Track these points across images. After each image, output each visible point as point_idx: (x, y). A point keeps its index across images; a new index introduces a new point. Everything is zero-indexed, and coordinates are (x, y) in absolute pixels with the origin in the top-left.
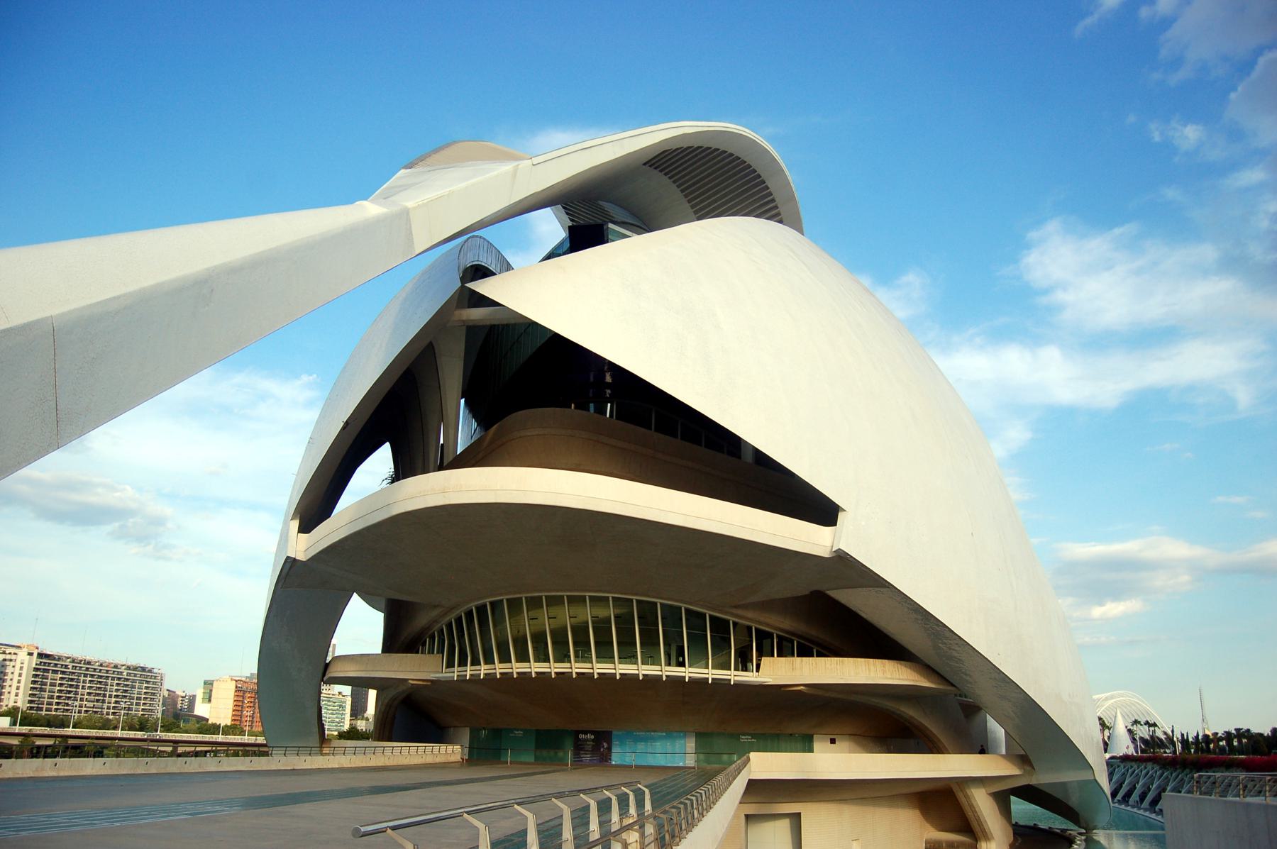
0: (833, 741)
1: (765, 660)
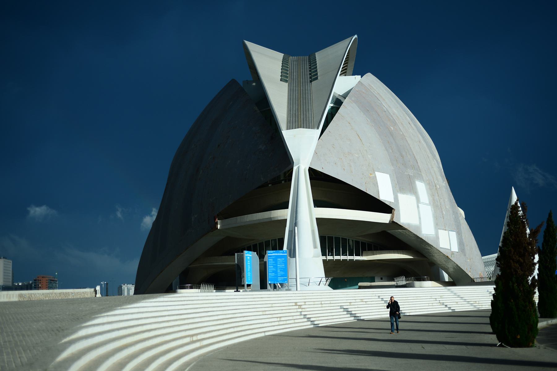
0: (382, 279)
1: (364, 252)
